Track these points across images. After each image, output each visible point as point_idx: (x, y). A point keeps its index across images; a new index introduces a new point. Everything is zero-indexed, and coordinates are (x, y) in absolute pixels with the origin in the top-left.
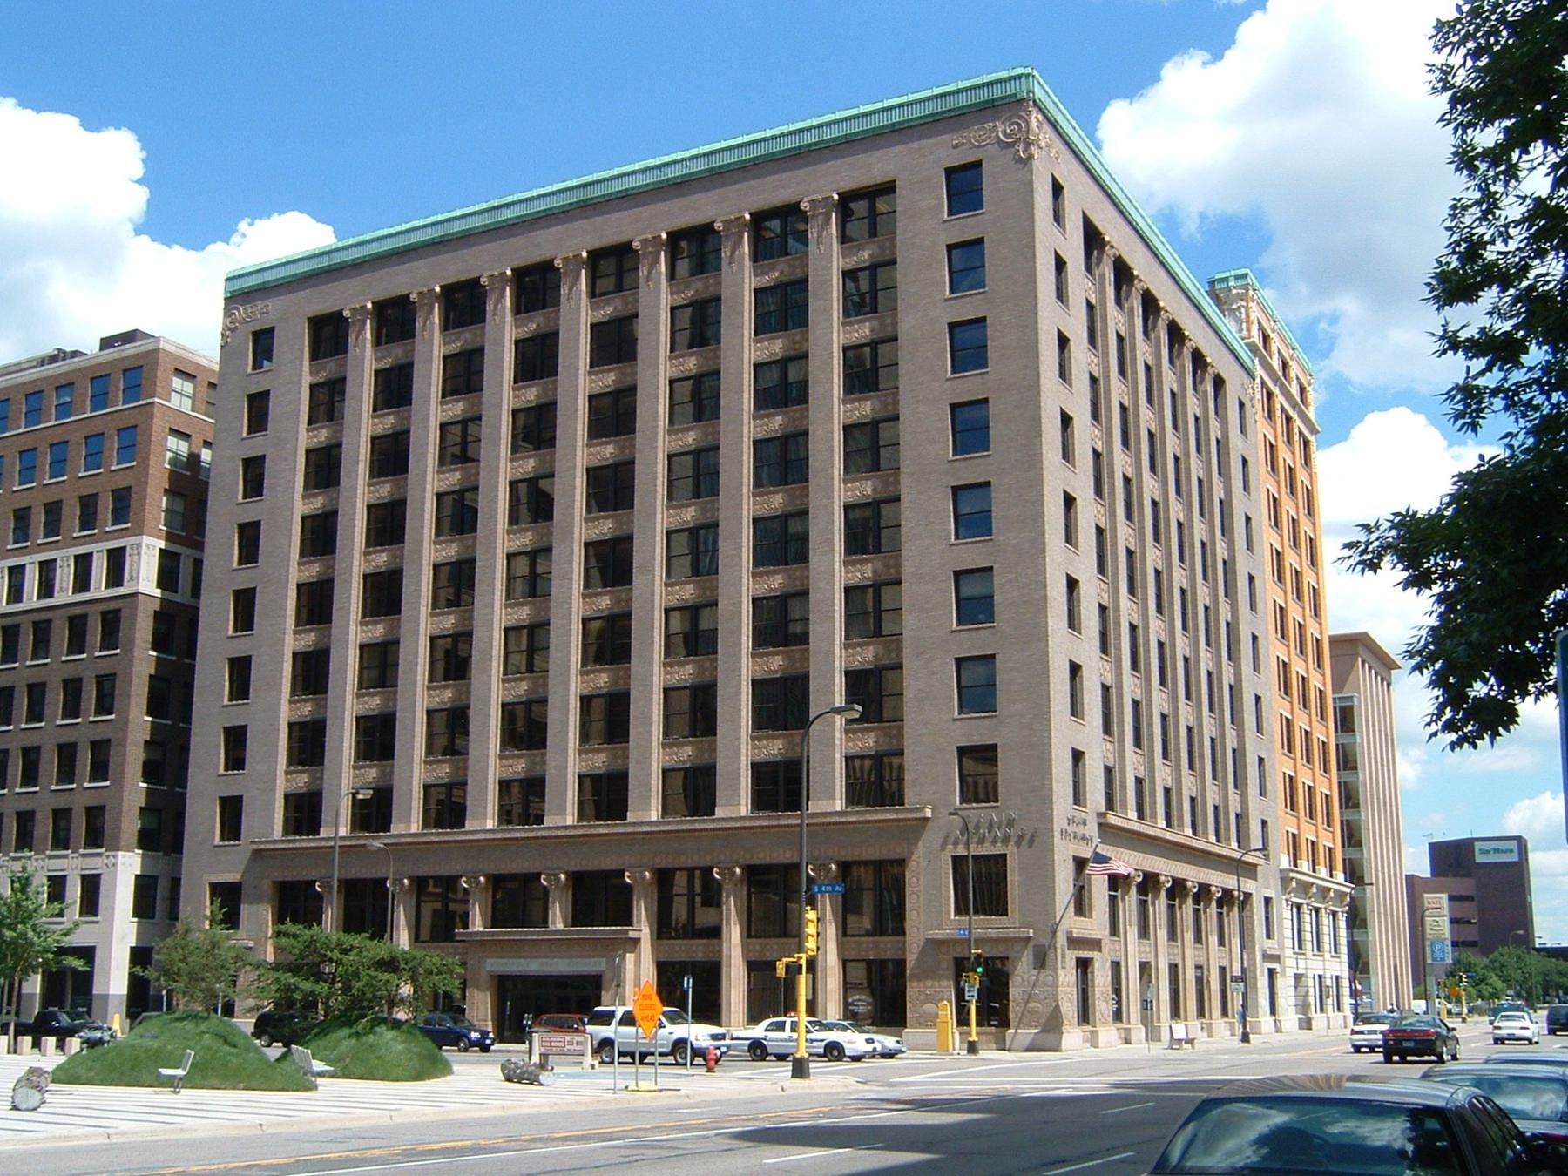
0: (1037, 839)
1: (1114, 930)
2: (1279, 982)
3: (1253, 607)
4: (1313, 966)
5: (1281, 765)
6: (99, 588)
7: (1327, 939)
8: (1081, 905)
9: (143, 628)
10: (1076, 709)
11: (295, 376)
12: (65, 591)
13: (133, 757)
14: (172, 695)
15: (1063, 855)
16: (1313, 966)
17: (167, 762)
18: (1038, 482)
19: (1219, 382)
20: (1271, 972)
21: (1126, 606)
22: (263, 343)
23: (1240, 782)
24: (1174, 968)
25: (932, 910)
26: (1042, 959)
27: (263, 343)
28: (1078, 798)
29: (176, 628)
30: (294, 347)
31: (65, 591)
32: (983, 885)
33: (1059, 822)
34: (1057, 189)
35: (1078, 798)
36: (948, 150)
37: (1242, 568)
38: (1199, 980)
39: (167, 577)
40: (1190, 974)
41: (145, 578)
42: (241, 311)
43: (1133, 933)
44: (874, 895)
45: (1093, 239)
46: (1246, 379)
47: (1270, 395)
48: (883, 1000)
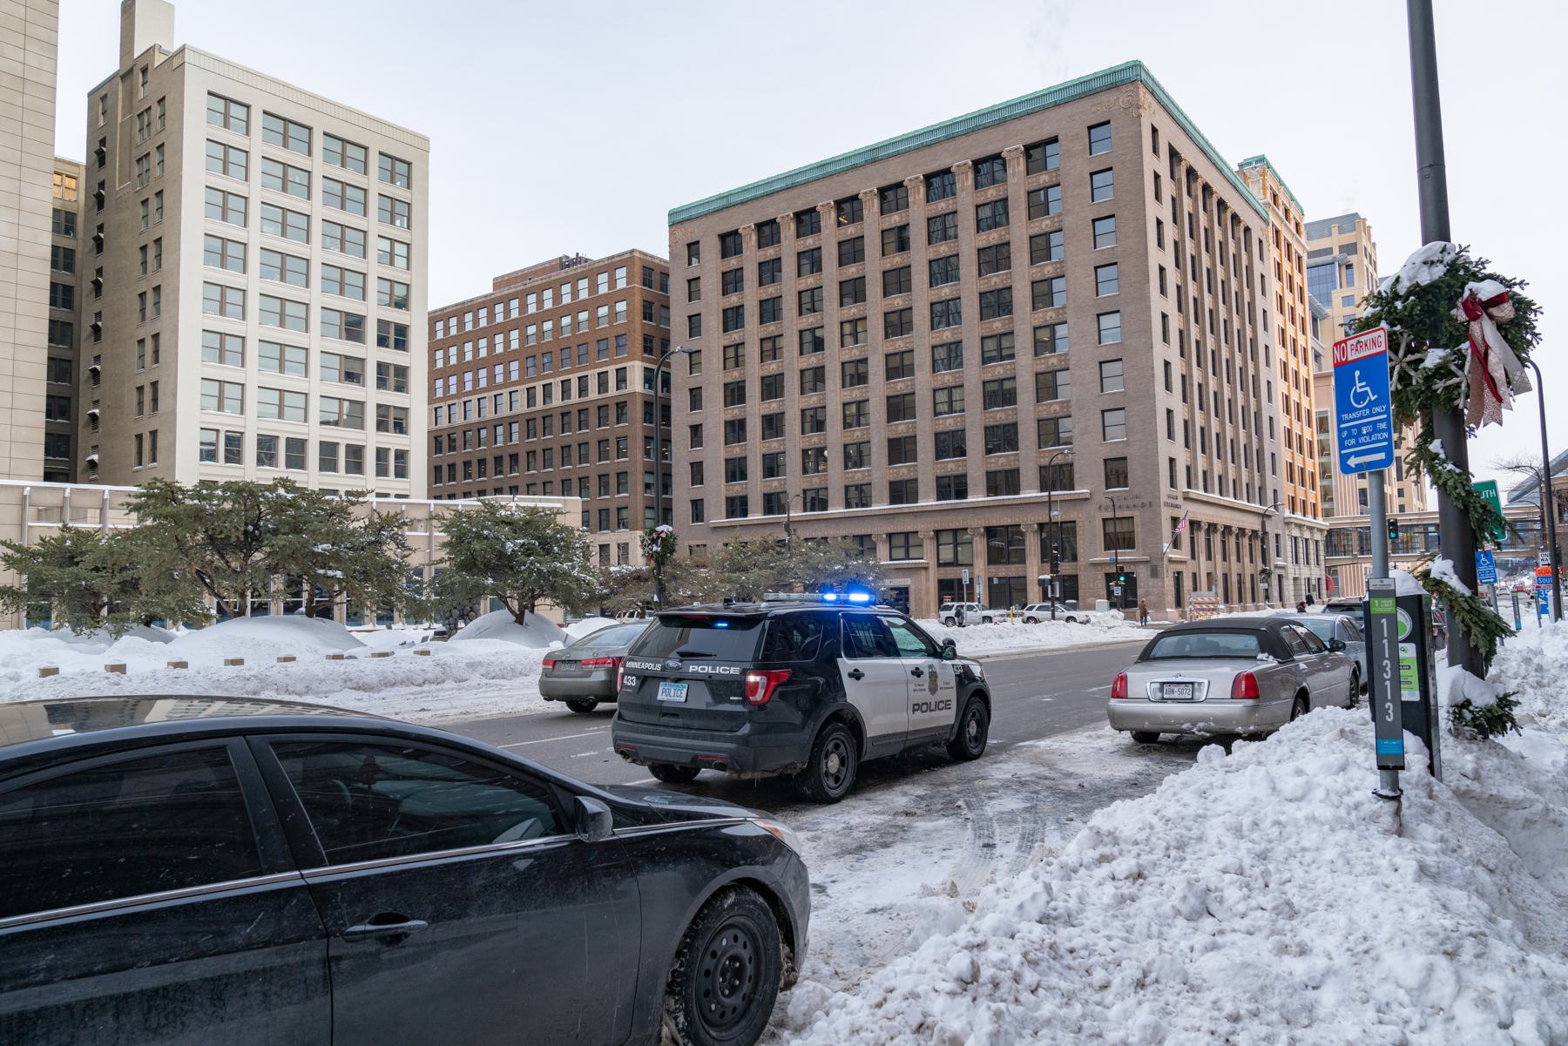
0: (1151, 505)
1: (1193, 557)
2: (1285, 583)
3: (1268, 364)
4: (1305, 572)
5: (1285, 455)
6: (612, 391)
7: (1312, 557)
8: (1176, 544)
9: (636, 411)
10: (1170, 435)
11: (711, 266)
12: (593, 394)
13: (638, 479)
14: (659, 442)
15: (1166, 514)
16: (1305, 572)
17: (663, 480)
18: (1149, 309)
19: (1247, 230)
20: (1280, 577)
21: (1196, 372)
22: (693, 248)
23: (1261, 468)
24: (1225, 576)
25: (1092, 552)
26: (1155, 573)
27: (693, 248)
28: (1173, 484)
29: (657, 411)
30: (710, 249)
31: (593, 394)
32: (1118, 539)
33: (1164, 498)
34: (1154, 131)
35: (1173, 484)
36: (1091, 111)
37: (1260, 304)
38: (1240, 582)
39: (649, 379)
40: (1234, 579)
41: (636, 383)
42: (679, 232)
43: (1203, 558)
44: (1059, 541)
45: (1174, 155)
46: (1263, 225)
47: (1277, 232)
48: (1067, 592)
